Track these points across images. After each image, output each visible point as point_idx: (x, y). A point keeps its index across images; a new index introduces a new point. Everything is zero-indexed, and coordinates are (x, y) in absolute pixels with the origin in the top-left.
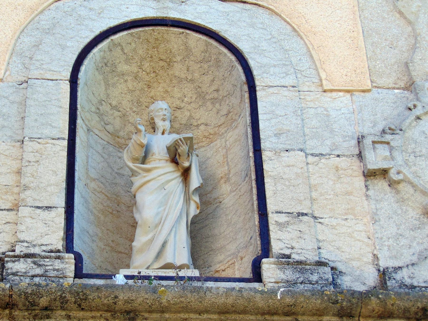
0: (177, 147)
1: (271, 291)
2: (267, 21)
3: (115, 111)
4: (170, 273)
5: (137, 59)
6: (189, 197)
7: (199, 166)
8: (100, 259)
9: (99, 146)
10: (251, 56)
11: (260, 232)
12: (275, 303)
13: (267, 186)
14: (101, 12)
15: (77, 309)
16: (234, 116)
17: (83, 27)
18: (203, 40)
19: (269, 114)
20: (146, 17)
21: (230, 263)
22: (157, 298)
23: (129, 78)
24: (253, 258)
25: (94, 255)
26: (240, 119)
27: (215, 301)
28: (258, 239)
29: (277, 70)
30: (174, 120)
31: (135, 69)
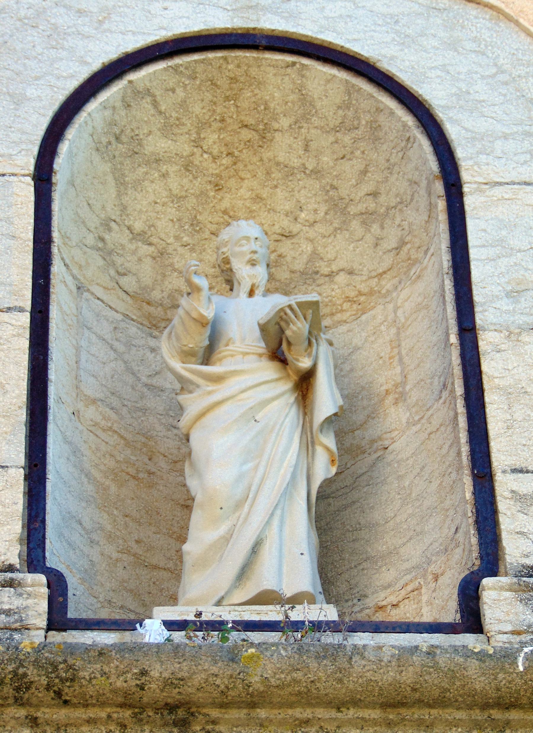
0: (283, 324)
1: (503, 653)
2: (486, 35)
3: (140, 244)
4: (270, 613)
5: (189, 125)
6: (312, 438)
7: (336, 367)
8: (108, 584)
9: (105, 323)
10: (451, 115)
11: (477, 517)
12: (513, 680)
13: (491, 411)
14: (105, 18)
15: (53, 702)
16: (413, 252)
17: (64, 54)
18: (341, 80)
19: (493, 247)
20: (208, 30)
21: (409, 588)
22: (239, 674)
23: (172, 169)
24: (463, 576)
25: (95, 574)
26: (426, 260)
27: (373, 678)
28: (473, 532)
29: (511, 145)
30: (276, 262)
31: (186, 149)
